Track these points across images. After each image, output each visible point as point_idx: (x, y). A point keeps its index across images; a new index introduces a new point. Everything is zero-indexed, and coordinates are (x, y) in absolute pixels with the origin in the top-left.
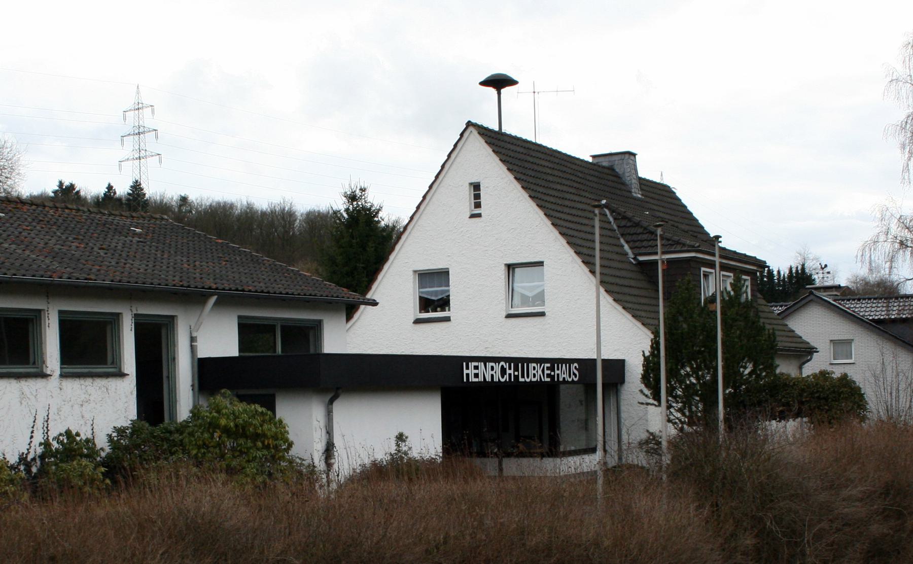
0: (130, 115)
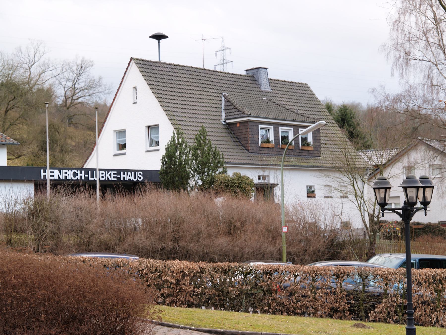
0: (219, 53)
